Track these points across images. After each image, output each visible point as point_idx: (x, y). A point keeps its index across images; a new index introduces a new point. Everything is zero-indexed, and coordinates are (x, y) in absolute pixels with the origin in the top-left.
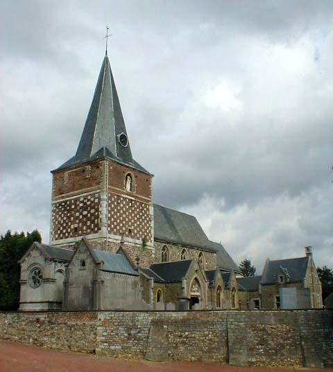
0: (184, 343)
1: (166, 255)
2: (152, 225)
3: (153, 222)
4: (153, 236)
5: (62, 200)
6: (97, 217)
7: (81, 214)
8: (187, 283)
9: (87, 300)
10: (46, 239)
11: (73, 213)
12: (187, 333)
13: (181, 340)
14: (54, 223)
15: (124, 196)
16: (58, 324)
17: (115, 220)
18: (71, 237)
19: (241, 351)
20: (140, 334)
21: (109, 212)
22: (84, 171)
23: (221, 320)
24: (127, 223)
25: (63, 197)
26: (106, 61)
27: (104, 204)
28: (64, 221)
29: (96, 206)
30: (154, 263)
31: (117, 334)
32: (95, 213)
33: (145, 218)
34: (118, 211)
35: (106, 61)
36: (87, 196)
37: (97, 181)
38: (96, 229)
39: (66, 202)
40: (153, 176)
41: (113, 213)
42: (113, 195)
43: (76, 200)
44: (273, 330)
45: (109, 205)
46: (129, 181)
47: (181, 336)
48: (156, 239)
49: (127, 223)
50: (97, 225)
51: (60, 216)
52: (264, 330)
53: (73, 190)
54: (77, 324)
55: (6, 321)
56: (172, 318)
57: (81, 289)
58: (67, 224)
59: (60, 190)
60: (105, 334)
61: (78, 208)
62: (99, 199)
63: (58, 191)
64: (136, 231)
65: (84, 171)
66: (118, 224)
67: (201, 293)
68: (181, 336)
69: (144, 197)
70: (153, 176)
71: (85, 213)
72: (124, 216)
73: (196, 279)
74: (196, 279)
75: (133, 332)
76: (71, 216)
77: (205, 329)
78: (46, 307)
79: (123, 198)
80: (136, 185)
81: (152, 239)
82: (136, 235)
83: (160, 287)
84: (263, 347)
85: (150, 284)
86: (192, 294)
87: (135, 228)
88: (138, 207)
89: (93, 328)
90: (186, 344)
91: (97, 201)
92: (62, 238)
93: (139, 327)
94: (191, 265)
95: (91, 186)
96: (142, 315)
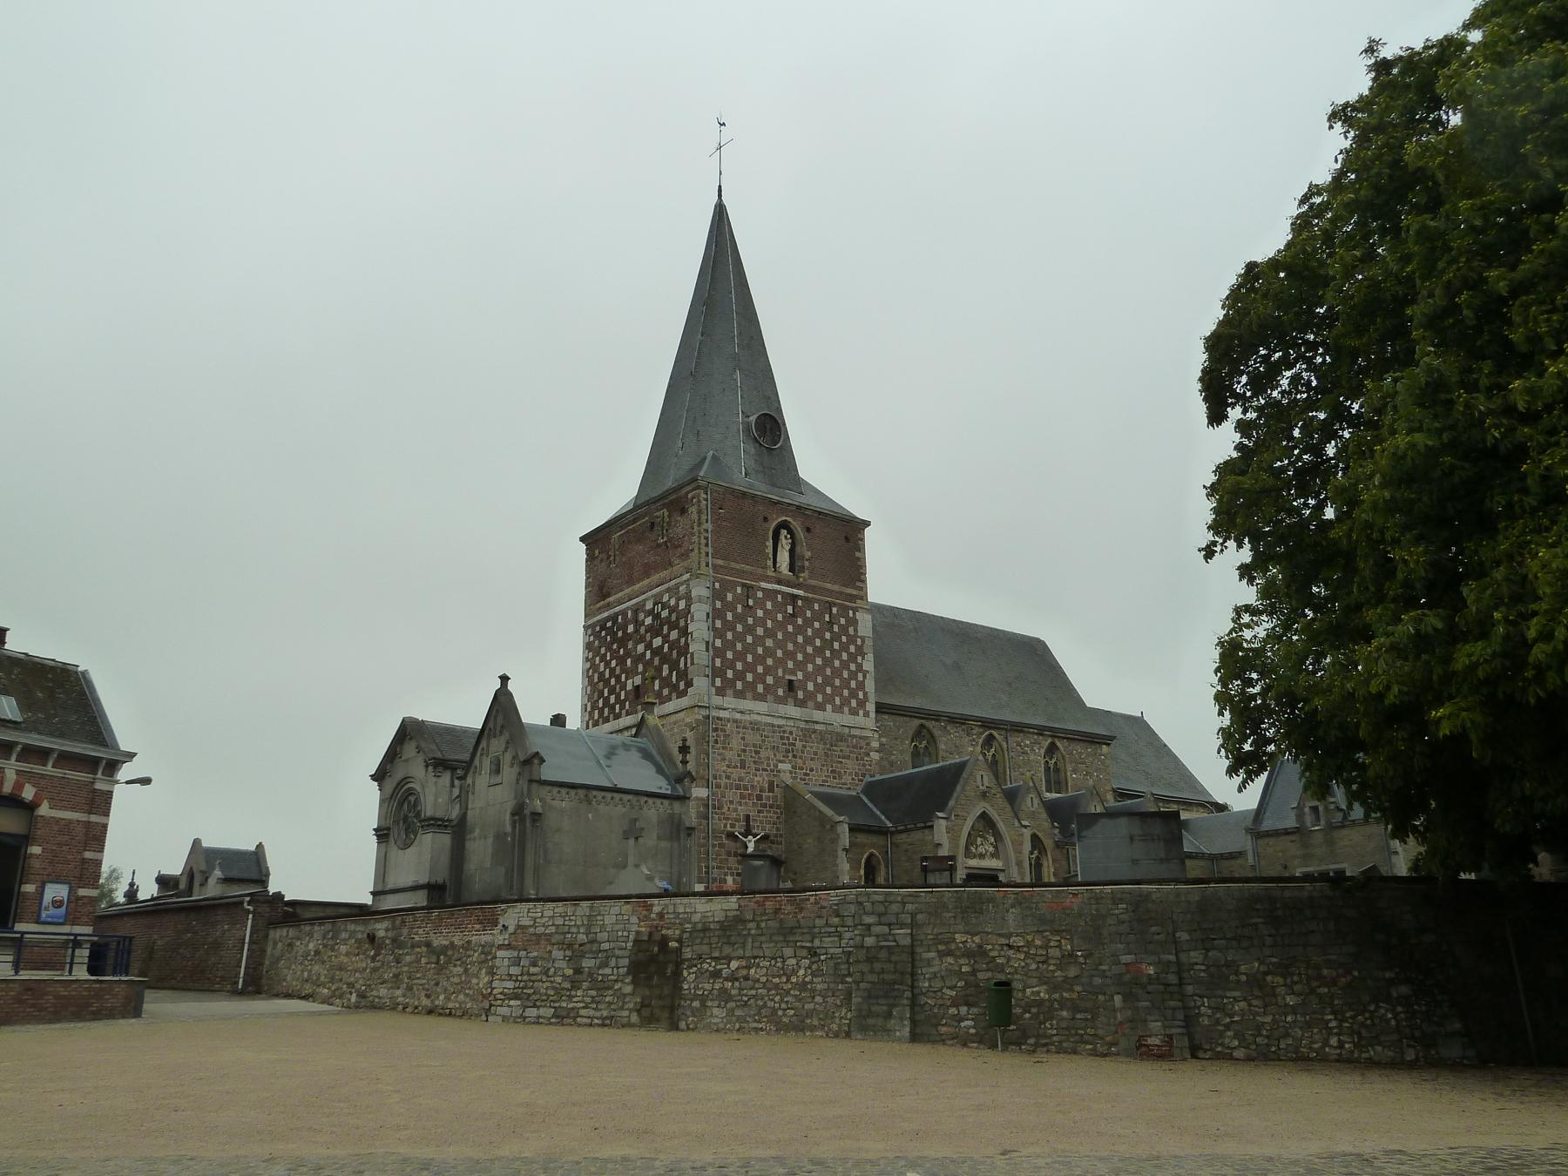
0: (725, 996)
1: (1057, 770)
3: (870, 657)
4: (872, 698)
5: (606, 614)
6: (684, 652)
7: (649, 646)
9: (502, 870)
10: (574, 722)
12: (734, 964)
14: (590, 678)
16: (413, 947)
17: (740, 656)
18: (628, 714)
20: (607, 971)
21: (719, 633)
23: (836, 920)
24: (781, 662)
25: (609, 607)
27: (700, 611)
28: (612, 671)
30: (878, 777)
31: (546, 973)
32: (678, 640)
36: (661, 595)
38: (682, 685)
39: (614, 618)
42: (727, 586)
43: (636, 610)
45: (717, 614)
46: (785, 543)
47: (716, 974)
48: (881, 709)
49: (781, 662)
50: (683, 675)
51: (603, 658)
52: (981, 952)
55: (311, 946)
56: (696, 918)
57: (490, 840)
58: (618, 678)
59: (601, 588)
60: (514, 970)
61: (642, 630)
62: (688, 598)
64: (810, 686)
65: (653, 524)
66: (750, 668)
67: (1007, 862)
68: (716, 974)
69: (829, 586)
70: (867, 524)
71: (657, 642)
72: (769, 643)
73: (984, 816)
74: (984, 816)
75: (587, 963)
76: (628, 654)
77: (788, 952)
78: (420, 899)
79: (763, 590)
80: (808, 554)
81: (871, 707)
82: (810, 696)
83: (872, 846)
84: (975, 1010)
85: (835, 840)
86: (973, 863)
87: (807, 677)
88: (817, 616)
89: (488, 951)
90: (730, 998)
91: (682, 605)
92: (607, 720)
95: (671, 564)
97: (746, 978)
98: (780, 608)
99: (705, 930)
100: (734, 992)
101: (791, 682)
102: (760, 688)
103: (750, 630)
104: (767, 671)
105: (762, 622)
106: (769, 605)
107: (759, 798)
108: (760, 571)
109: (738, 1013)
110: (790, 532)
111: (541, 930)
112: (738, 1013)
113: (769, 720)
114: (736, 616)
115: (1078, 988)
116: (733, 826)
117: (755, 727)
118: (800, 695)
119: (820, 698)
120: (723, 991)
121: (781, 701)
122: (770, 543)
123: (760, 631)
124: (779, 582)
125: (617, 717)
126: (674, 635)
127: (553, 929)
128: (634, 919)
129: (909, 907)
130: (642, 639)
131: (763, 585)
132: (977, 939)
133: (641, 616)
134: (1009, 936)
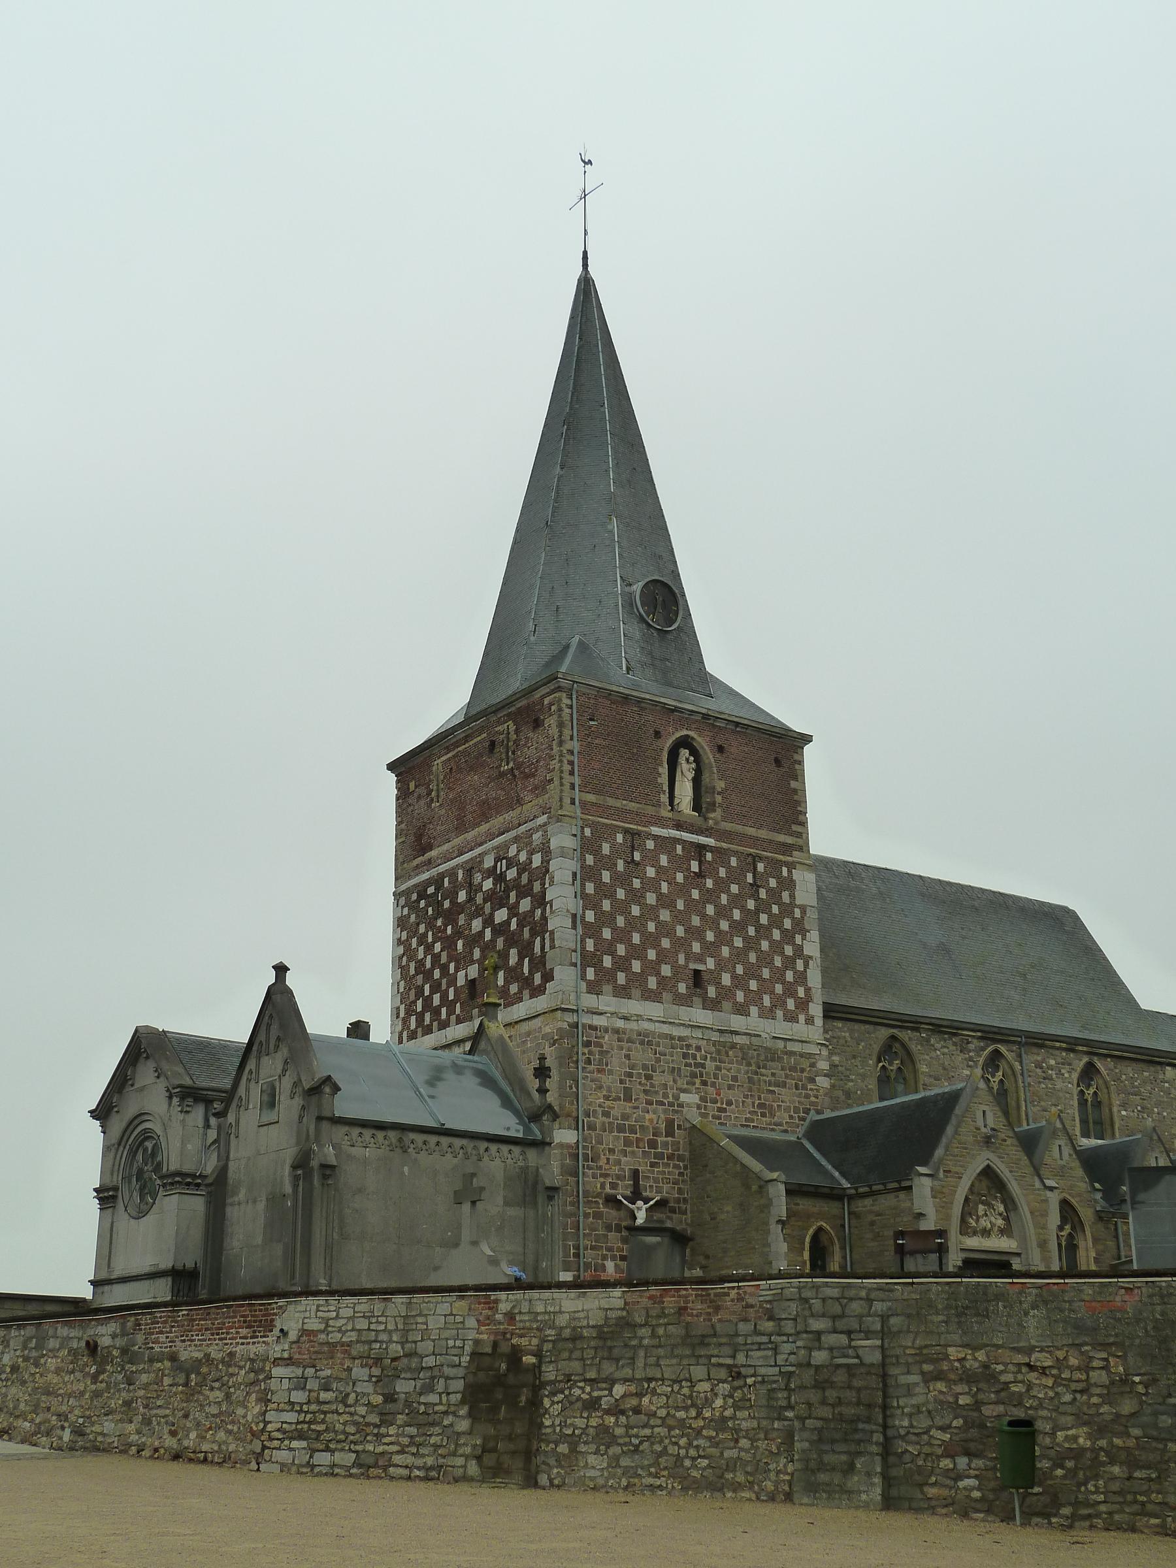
0: (605, 1437)
1: (1098, 1104)
2: (812, 947)
3: (814, 935)
5: (425, 876)
6: (540, 929)
7: (489, 921)
8: (935, 1193)
9: (279, 1249)
11: (462, 920)
12: (619, 1390)
13: (594, 1422)
14: (404, 969)
15: (664, 832)
16: (151, 1361)
17: (622, 936)
18: (459, 1021)
19: (854, 1481)
20: (433, 1398)
22: (493, 744)
23: (769, 1326)
24: (681, 944)
25: (429, 863)
26: (586, 291)
27: (562, 869)
29: (532, 885)
32: (532, 912)
33: (776, 922)
34: (636, 896)
35: (586, 291)
36: (506, 846)
37: (535, 781)
39: (438, 881)
40: (807, 739)
41: (606, 905)
43: (470, 869)
44: (1033, 1376)
45: (587, 874)
46: (686, 770)
47: (592, 1405)
48: (831, 1012)
50: (539, 963)
51: (422, 940)
52: (987, 1375)
53: (461, 828)
54: (207, 1356)
56: (562, 1321)
57: (261, 1206)
58: (444, 969)
59: (419, 837)
60: (298, 1396)
61: (479, 899)
62: (546, 850)
63: (414, 842)
64: (726, 979)
66: (637, 952)
67: (1023, 1240)
68: (592, 1405)
70: (807, 739)
71: (501, 915)
73: (988, 1173)
74: (988, 1173)
75: (403, 1387)
77: (699, 1372)
79: (656, 838)
80: (720, 785)
81: (816, 1010)
82: (726, 994)
84: (979, 1463)
86: (973, 1242)
88: (735, 876)
89: (259, 1368)
90: (613, 1440)
91: (537, 860)
92: (428, 1030)
93: (430, 1361)
94: (958, 1111)
95: (520, 802)
96: (444, 1308)
97: (637, 1411)
98: (679, 863)
99: (575, 1338)
100: (619, 1431)
101: (697, 973)
102: (652, 982)
103: (636, 896)
104: (663, 956)
105: (653, 885)
106: (664, 860)
107: (653, 1144)
108: (650, 810)
109: (625, 1462)
110: (694, 752)
111: (335, 1337)
112: (625, 1462)
113: (666, 1029)
114: (615, 876)
115: (1136, 1432)
116: (614, 1186)
117: (645, 1039)
118: (712, 992)
119: (740, 996)
120: (603, 1430)
121: (683, 1001)
122: (664, 770)
123: (651, 899)
124: (679, 826)
125: (444, 1025)
126: (525, 905)
127: (353, 1336)
128: (472, 1322)
129: (878, 1307)
130: (479, 912)
131: (655, 830)
132: (981, 1356)
133: (478, 878)
134: (1030, 1350)
